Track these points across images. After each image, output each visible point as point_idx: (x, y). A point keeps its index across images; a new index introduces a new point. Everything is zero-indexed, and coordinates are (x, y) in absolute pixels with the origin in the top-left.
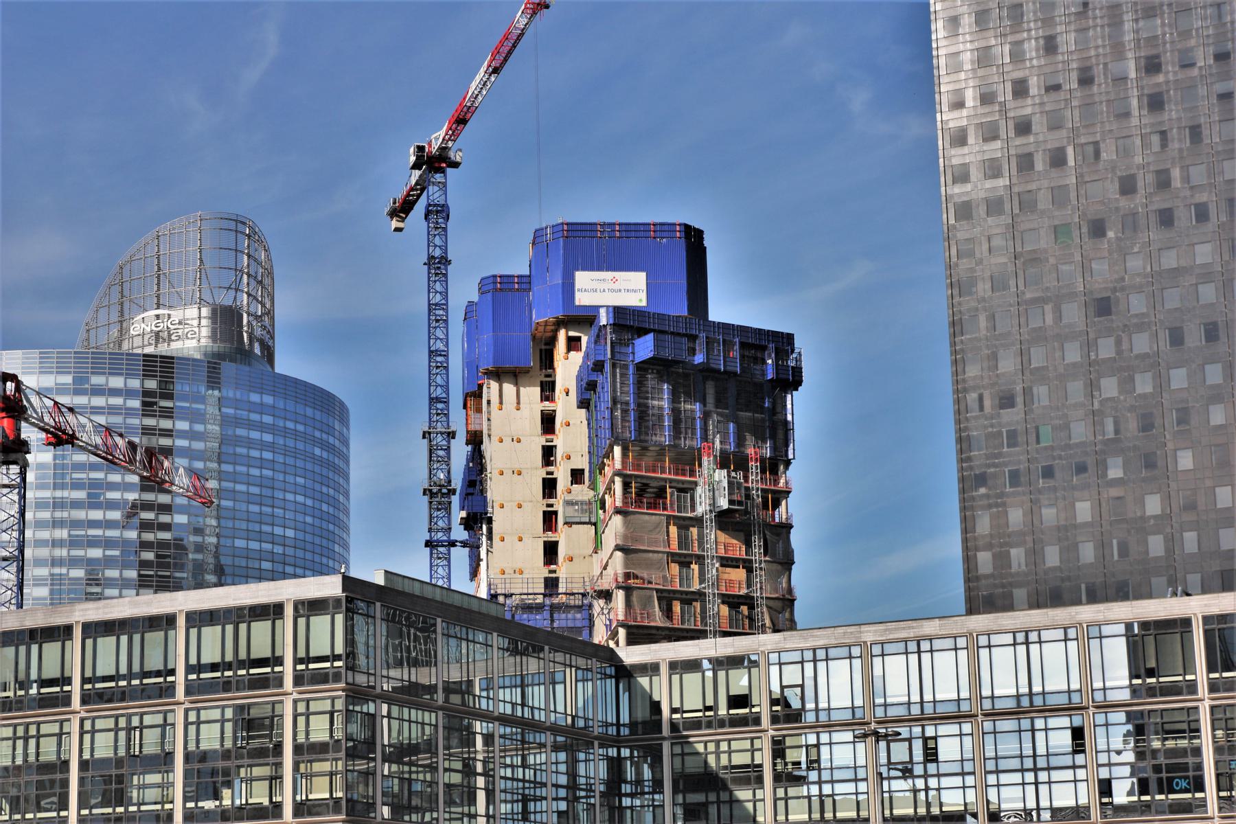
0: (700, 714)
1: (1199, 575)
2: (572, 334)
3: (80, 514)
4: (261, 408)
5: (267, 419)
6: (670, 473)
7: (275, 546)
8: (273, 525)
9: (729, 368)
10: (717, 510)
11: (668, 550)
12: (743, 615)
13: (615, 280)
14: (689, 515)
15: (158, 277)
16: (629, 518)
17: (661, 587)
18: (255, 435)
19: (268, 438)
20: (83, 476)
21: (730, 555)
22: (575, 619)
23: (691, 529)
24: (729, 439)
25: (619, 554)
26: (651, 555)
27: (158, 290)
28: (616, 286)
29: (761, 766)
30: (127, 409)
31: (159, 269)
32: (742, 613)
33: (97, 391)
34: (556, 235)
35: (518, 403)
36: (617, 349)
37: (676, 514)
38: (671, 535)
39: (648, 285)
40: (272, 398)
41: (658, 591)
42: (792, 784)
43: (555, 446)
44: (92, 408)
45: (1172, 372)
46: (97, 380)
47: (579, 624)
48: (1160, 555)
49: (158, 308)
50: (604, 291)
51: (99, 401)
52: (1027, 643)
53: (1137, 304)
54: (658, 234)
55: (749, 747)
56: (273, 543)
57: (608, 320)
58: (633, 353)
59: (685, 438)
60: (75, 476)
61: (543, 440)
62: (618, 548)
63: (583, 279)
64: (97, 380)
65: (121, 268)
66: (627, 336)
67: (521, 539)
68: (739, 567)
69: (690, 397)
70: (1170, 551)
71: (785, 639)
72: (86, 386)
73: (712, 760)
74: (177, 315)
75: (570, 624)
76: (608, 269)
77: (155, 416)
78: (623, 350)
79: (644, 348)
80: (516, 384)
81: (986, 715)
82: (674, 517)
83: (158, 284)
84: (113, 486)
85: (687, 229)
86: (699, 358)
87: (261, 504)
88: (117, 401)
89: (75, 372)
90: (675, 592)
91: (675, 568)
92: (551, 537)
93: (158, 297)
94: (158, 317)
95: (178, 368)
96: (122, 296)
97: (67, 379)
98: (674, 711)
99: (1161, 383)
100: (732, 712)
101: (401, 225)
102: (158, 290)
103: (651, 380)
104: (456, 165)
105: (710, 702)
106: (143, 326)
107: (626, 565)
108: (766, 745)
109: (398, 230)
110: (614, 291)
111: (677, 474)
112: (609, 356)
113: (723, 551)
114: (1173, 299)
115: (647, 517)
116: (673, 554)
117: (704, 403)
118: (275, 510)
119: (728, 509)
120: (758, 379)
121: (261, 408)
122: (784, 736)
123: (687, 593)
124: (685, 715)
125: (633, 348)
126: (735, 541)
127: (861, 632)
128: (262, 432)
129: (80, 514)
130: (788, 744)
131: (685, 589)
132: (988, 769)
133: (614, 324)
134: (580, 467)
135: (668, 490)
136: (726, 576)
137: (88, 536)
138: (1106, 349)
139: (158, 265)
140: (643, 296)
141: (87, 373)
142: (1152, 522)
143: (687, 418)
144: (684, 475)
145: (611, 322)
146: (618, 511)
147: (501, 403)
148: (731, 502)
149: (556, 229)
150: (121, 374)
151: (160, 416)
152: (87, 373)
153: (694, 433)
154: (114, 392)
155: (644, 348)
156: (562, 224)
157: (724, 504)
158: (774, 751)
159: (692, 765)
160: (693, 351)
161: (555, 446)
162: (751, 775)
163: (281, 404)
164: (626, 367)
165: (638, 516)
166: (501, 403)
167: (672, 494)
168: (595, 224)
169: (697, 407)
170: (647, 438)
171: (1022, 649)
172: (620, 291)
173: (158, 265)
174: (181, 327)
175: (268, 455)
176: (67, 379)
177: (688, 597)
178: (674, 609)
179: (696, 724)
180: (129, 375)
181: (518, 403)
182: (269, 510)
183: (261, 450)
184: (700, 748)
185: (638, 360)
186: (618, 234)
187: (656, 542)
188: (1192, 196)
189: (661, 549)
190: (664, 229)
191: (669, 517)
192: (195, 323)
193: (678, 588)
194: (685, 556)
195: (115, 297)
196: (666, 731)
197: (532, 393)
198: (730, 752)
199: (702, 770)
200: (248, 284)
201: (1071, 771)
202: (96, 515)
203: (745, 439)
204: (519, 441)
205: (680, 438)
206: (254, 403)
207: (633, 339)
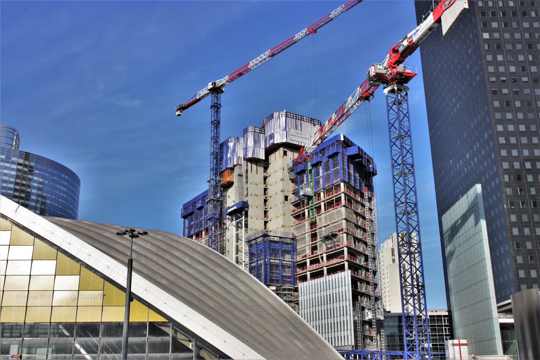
2: (285, 150)
4: (64, 180)
5: (66, 184)
18: (62, 188)
19: (65, 190)
22: (288, 248)
25: (344, 221)
28: (302, 136)
35: (257, 172)
43: (268, 189)
47: (290, 249)
61: (8, 221)
62: (345, 219)
67: (257, 219)
72: (10, 160)
75: (287, 249)
80: (256, 165)
89: (6, 155)
92: (266, 219)
101: (181, 113)
107: (347, 226)
109: (179, 115)
121: (64, 180)
133: (343, 141)
134: (287, 195)
141: (11, 156)
146: (344, 206)
147: (252, 171)
152: (11, 156)
161: (268, 189)
163: (69, 180)
166: (252, 171)
181: (257, 172)
197: (261, 169)
204: (257, 185)
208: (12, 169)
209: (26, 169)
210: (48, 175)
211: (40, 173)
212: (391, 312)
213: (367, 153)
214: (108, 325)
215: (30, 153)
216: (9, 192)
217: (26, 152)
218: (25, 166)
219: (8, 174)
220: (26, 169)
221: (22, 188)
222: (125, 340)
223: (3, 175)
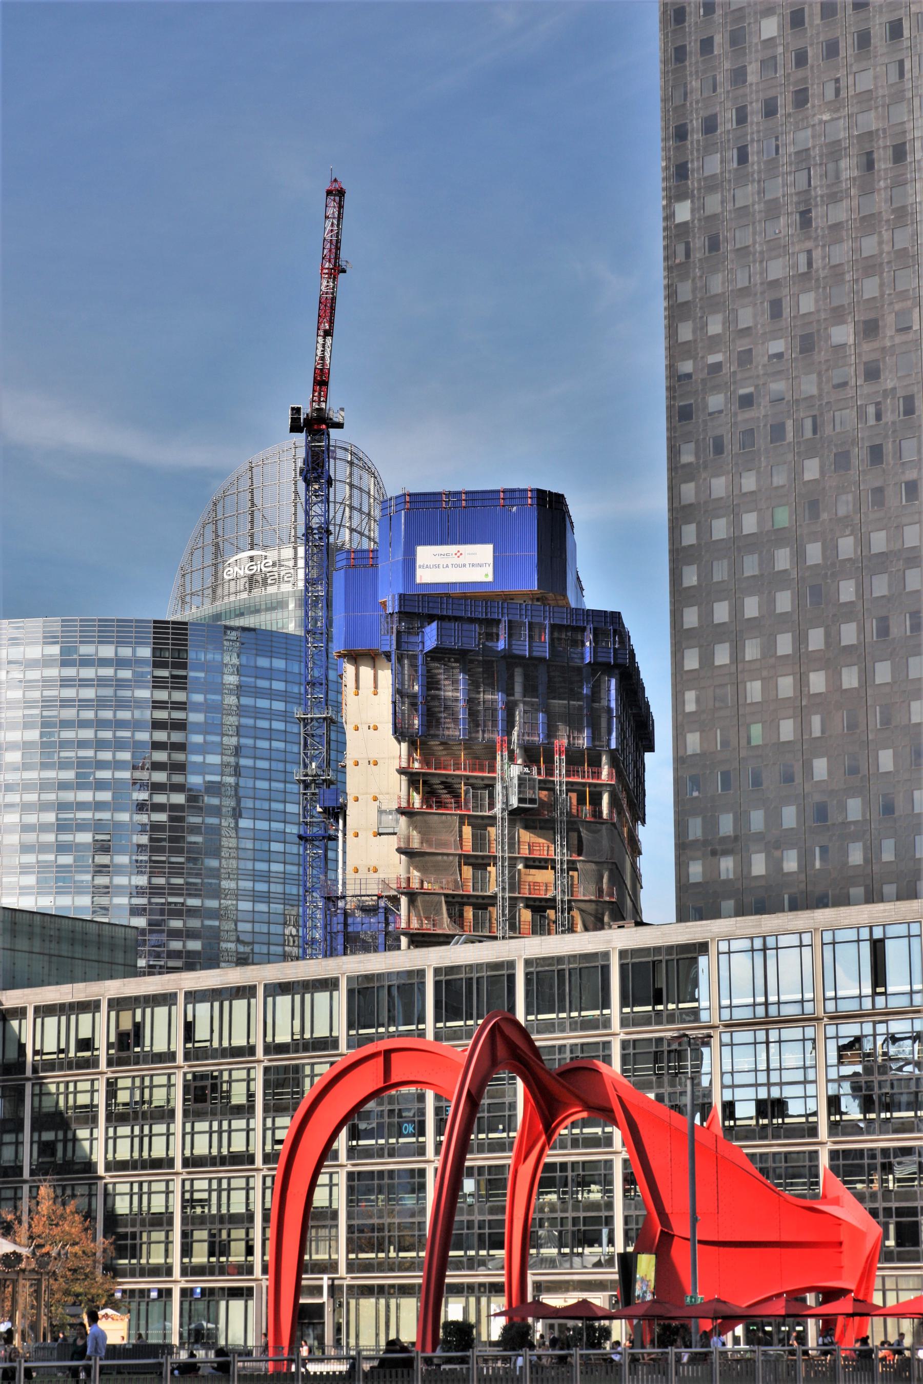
0: (54, 1056)
1: (895, 885)
3: (68, 796)
5: (278, 686)
6: (465, 769)
7: (288, 826)
8: (285, 802)
9: (535, 654)
10: (510, 808)
11: (459, 852)
12: (549, 920)
13: (459, 554)
14: (487, 814)
15: (252, 514)
16: (415, 818)
17: (451, 892)
18: (263, 703)
19: (279, 706)
20: (72, 754)
21: (536, 855)
23: (489, 829)
24: (538, 729)
26: (440, 858)
27: (252, 528)
28: (461, 561)
29: (97, 1106)
30: (117, 680)
31: (253, 505)
32: (548, 918)
33: (85, 662)
34: (399, 507)
35: (376, 687)
36: (404, 638)
37: (471, 813)
38: (464, 836)
39: (495, 557)
40: (283, 662)
41: (446, 896)
42: (280, 1114)
44: (80, 680)
45: (878, 665)
46: (86, 650)
48: (858, 863)
49: (252, 549)
50: (447, 566)
51: (88, 673)
52: (765, 949)
53: (847, 591)
54: (508, 501)
55: (245, 1076)
56: (285, 822)
57: (394, 608)
58: (423, 643)
59: (484, 732)
60: (63, 754)
63: (425, 554)
64: (86, 650)
65: (215, 504)
66: (417, 624)
68: (547, 868)
69: (491, 686)
70: (868, 860)
71: (124, 985)
72: (75, 657)
73: (62, 1103)
74: (272, 555)
76: (453, 542)
77: (167, 688)
78: (413, 639)
79: (430, 636)
80: (374, 667)
81: (831, 1018)
82: (469, 816)
83: (252, 522)
84: (101, 765)
85: (541, 495)
86: (501, 645)
87: (270, 780)
88: (108, 672)
90: (469, 896)
91: (468, 871)
93: (252, 536)
94: (252, 558)
95: (191, 629)
96: (217, 536)
97: (55, 650)
98: (36, 1052)
99: (866, 676)
100: (79, 1054)
102: (252, 528)
103: (440, 672)
104: (340, 426)
105: (63, 1046)
106: (236, 569)
108: (101, 1085)
110: (458, 566)
111: (472, 770)
112: (394, 647)
113: (527, 852)
114: (880, 586)
115: (436, 817)
116: (467, 857)
117: (509, 692)
118: (288, 785)
119: (518, 807)
120: (577, 663)
122: (116, 1079)
123: (483, 897)
124: (45, 1057)
125: (423, 637)
126: (542, 841)
127: (181, 979)
128: (271, 699)
129: (68, 796)
130: (120, 1085)
131: (480, 893)
132: (830, 1077)
135: (463, 788)
136: (530, 879)
137: (76, 819)
138: (816, 639)
139: (252, 500)
140: (490, 570)
141: (76, 642)
142: (853, 828)
143: (485, 710)
144: (482, 770)
145: (397, 610)
147: (357, 688)
148: (521, 800)
149: (399, 501)
150: (112, 642)
151: (173, 688)
152: (76, 642)
153: (495, 725)
154: (104, 662)
155: (430, 636)
156: (404, 495)
157: (514, 802)
158: (107, 1092)
159: (48, 1104)
160: (496, 637)
162: (88, 1115)
164: (415, 657)
165: (431, 817)
166: (357, 688)
167: (467, 792)
168: (440, 494)
169: (499, 697)
170: (437, 732)
171: (759, 957)
172: (465, 565)
173: (252, 500)
174: (275, 569)
175: (278, 725)
176: (55, 650)
177: (485, 901)
178: (465, 914)
179: (50, 1066)
180: (119, 643)
181: (376, 687)
182: (280, 786)
183: (271, 720)
184: (53, 1088)
185: (427, 649)
186: (464, 503)
187: (445, 844)
188: (903, 473)
189: (452, 851)
190: (512, 495)
191: (462, 817)
192: (291, 563)
193: (472, 893)
194: (483, 857)
195: (209, 537)
196: (29, 1072)
198: (75, 1093)
199: (53, 1109)
200: (350, 517)
201: (801, 1087)
202: (86, 796)
203: (557, 730)
204: (376, 728)
205: (478, 732)
206: (263, 668)
207: (422, 627)
208: (84, 683)
209: (126, 674)
210: (202, 675)
211: (173, 677)
212: (648, 756)
213: (660, 154)
214: (857, 103)
215: (185, 623)
216: (83, 753)
217: (155, 622)
218: (120, 663)
219: (74, 701)
220: (126, 674)
221: (120, 734)
222: (308, 1235)
223: (61, 706)
